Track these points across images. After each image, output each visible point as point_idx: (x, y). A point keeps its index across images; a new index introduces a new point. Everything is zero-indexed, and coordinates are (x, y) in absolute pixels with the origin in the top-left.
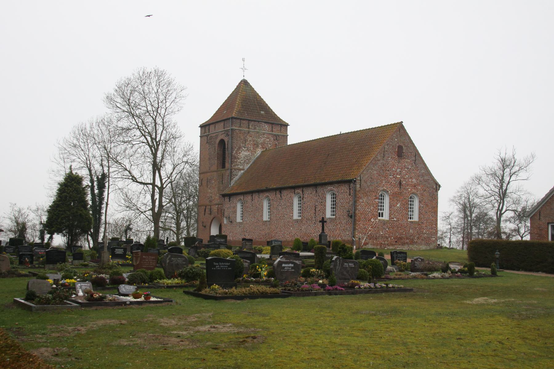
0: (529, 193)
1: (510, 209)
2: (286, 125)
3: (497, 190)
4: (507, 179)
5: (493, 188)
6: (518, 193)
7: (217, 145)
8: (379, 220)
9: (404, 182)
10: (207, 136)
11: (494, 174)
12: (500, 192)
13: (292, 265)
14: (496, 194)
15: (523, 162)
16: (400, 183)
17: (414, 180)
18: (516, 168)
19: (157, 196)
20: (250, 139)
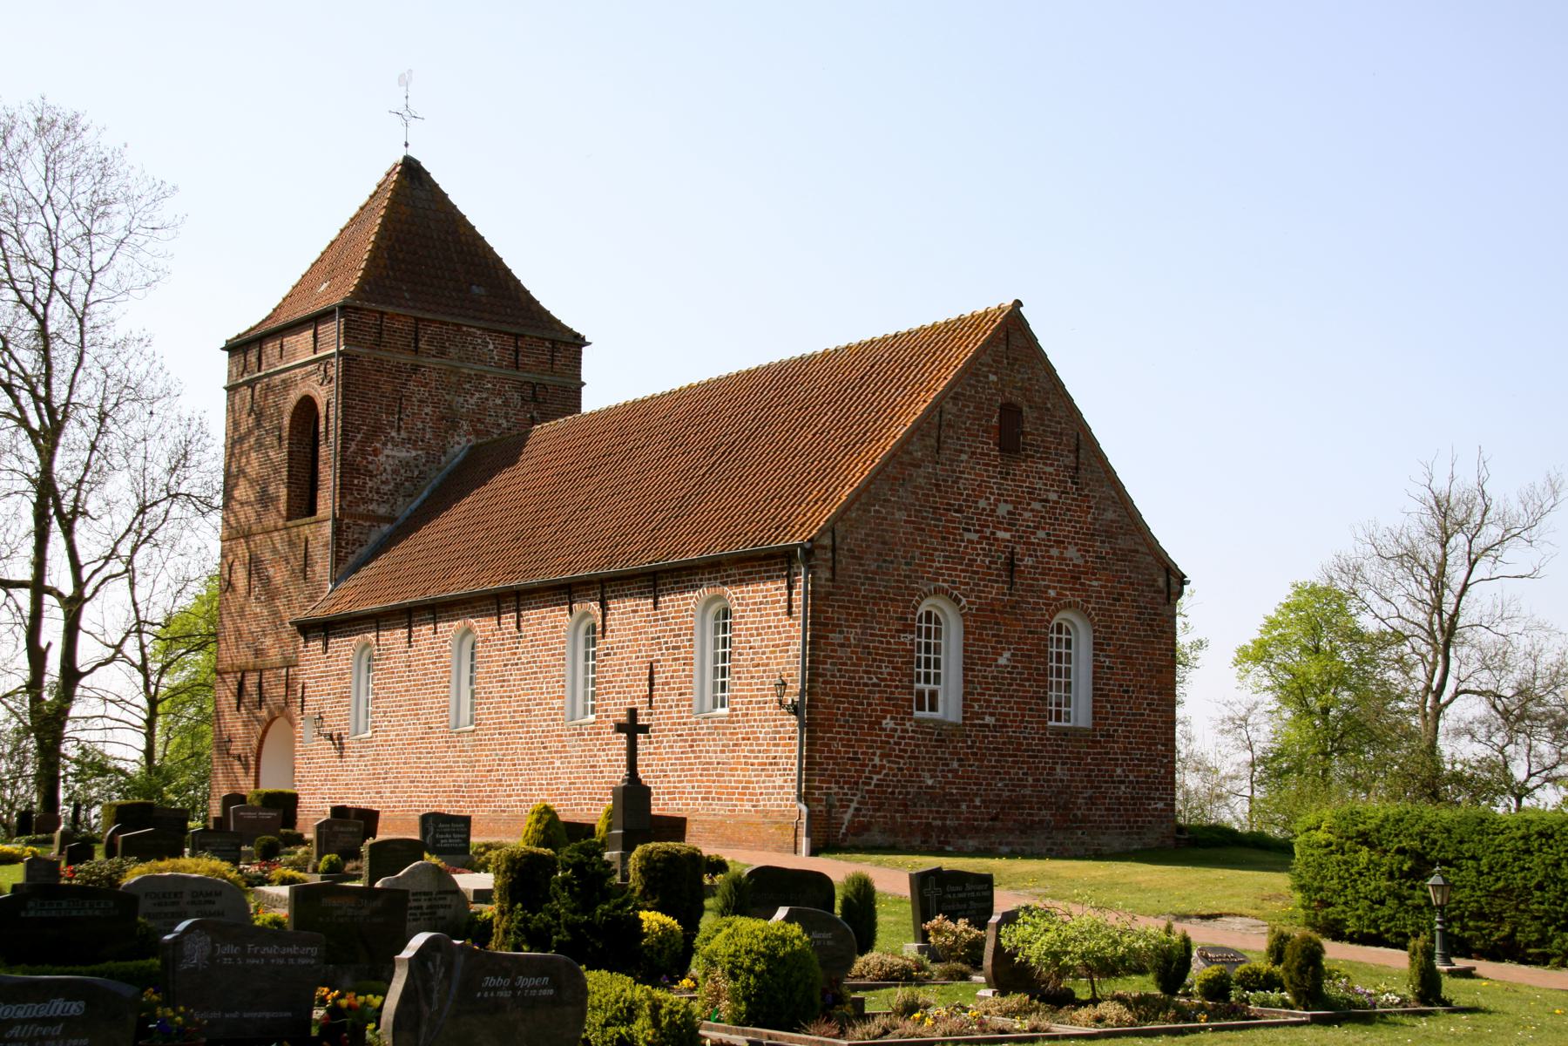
0: (1541, 627)
1: (1473, 687)
2: (578, 342)
3: (1421, 617)
4: (1456, 575)
5: (1407, 609)
6: (1502, 629)
7: (286, 421)
8: (919, 722)
9: (1028, 561)
10: (251, 384)
11: (1408, 558)
12: (1431, 624)
13: (76, 1008)
14: (1418, 631)
15: (1515, 507)
16: (1011, 565)
17: (1071, 552)
18: (1491, 533)
19: (52, 631)
20: (423, 393)
